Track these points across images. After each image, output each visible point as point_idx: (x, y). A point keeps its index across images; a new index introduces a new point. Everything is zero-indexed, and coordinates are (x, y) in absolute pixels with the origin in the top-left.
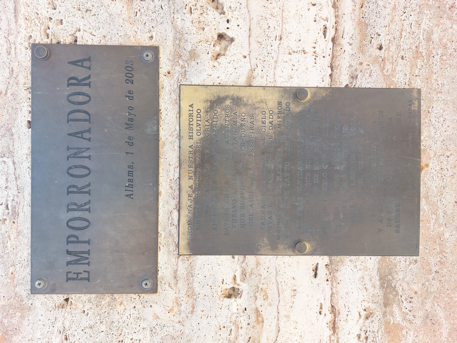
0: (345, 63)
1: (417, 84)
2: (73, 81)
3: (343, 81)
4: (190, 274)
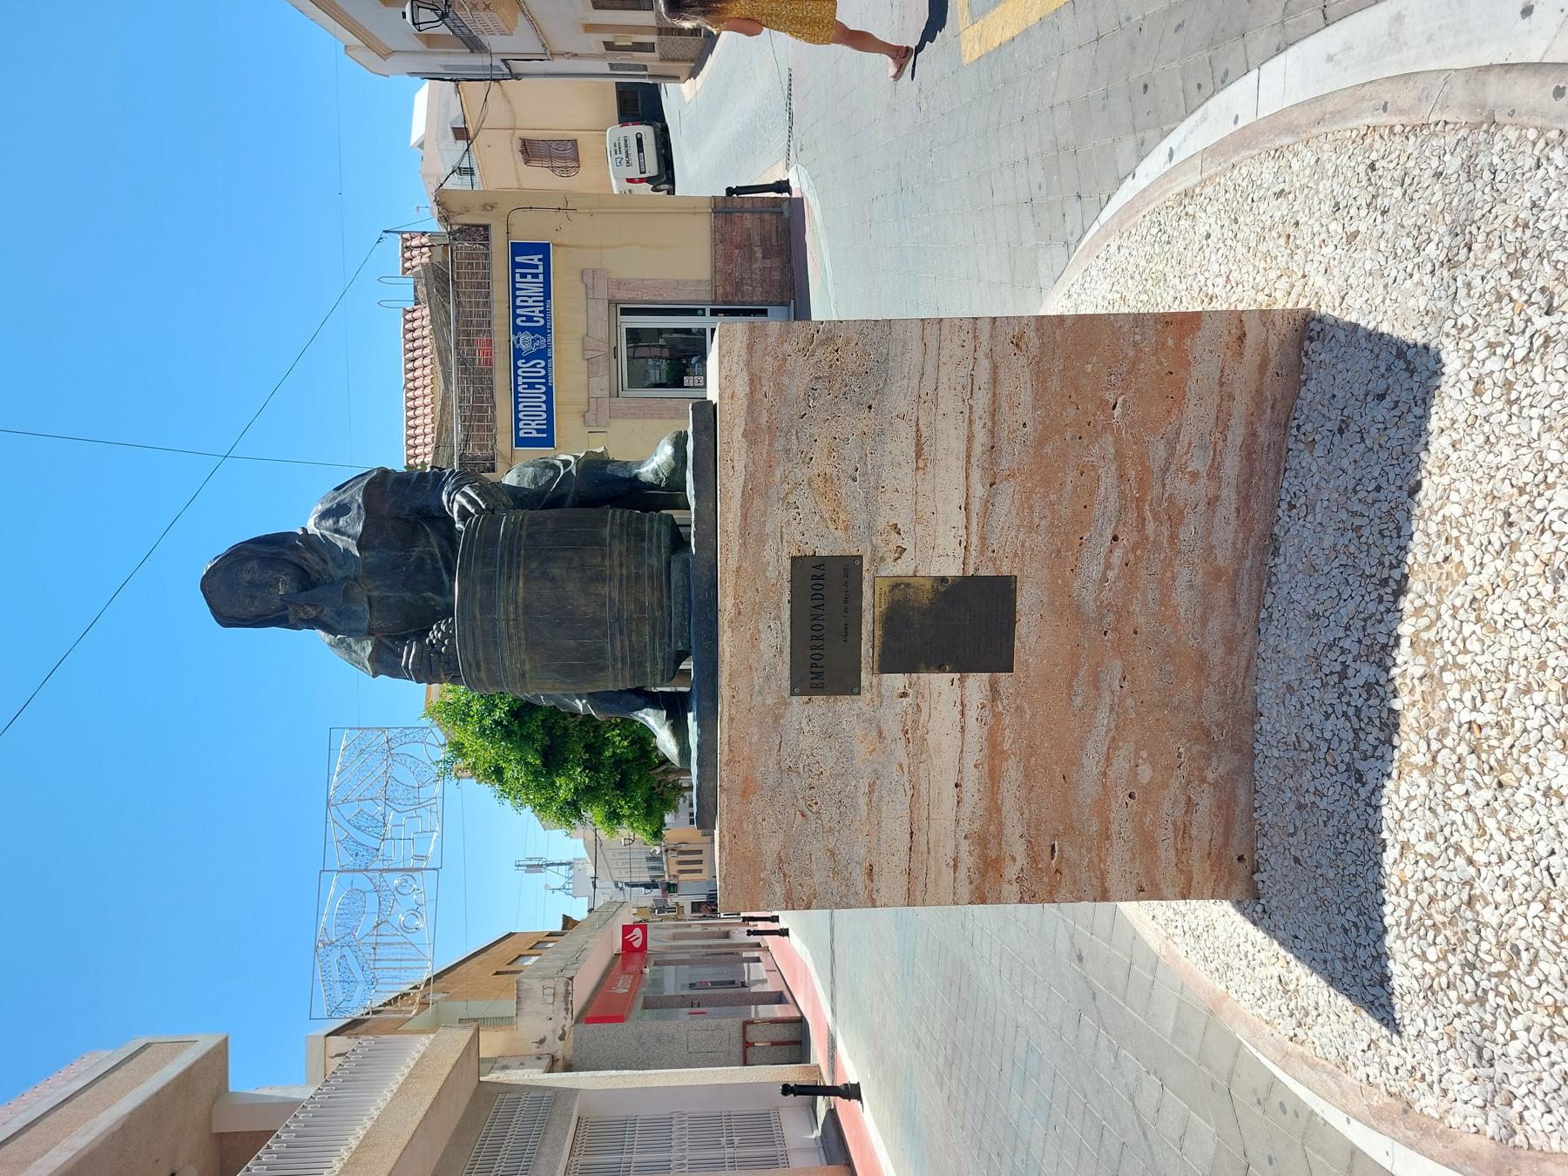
0: (971, 561)
1: (1015, 573)
2: (814, 577)
3: (971, 572)
4: (880, 684)
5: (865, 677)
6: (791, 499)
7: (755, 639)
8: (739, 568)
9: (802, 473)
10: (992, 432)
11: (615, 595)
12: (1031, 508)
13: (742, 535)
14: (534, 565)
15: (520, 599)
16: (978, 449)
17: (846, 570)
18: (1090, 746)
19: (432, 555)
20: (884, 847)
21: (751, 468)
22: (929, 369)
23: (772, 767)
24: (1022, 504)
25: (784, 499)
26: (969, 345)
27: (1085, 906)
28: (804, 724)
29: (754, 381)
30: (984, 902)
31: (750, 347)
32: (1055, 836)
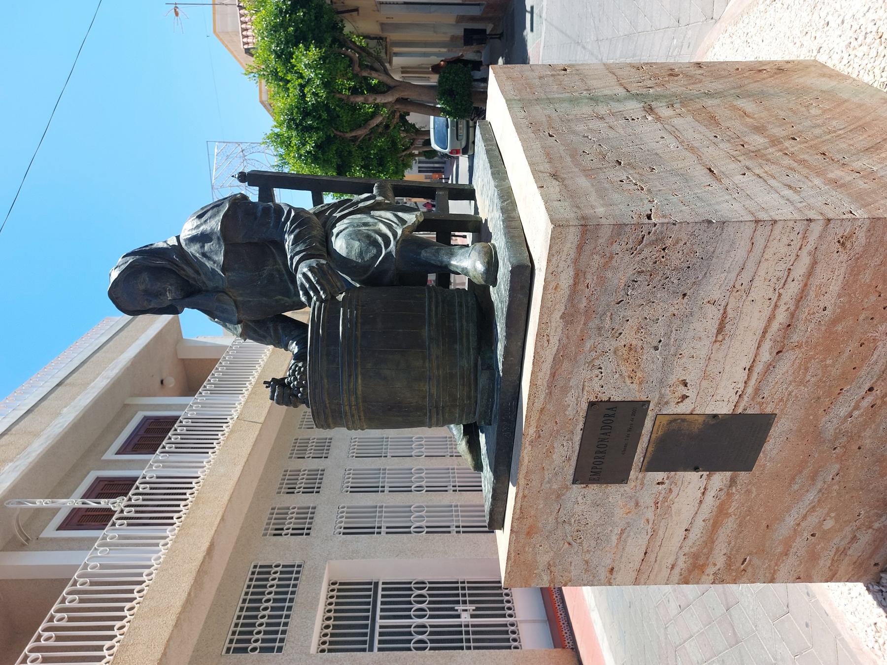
1: (777, 412)
4: (644, 477)
5: (633, 474)
6: (597, 362)
7: (550, 452)
8: (542, 410)
9: (610, 344)
10: (792, 315)
11: (434, 391)
12: (807, 369)
13: (549, 387)
14: (369, 366)
15: (359, 392)
16: (775, 326)
17: (634, 413)
18: (794, 512)
19: (279, 271)
20: (623, 559)
21: (565, 341)
22: (751, 266)
23: (551, 519)
24: (800, 368)
25: (589, 363)
26: (796, 244)
27: (759, 586)
28: (580, 499)
29: (578, 276)
30: (687, 583)
31: (580, 248)
32: (750, 554)
